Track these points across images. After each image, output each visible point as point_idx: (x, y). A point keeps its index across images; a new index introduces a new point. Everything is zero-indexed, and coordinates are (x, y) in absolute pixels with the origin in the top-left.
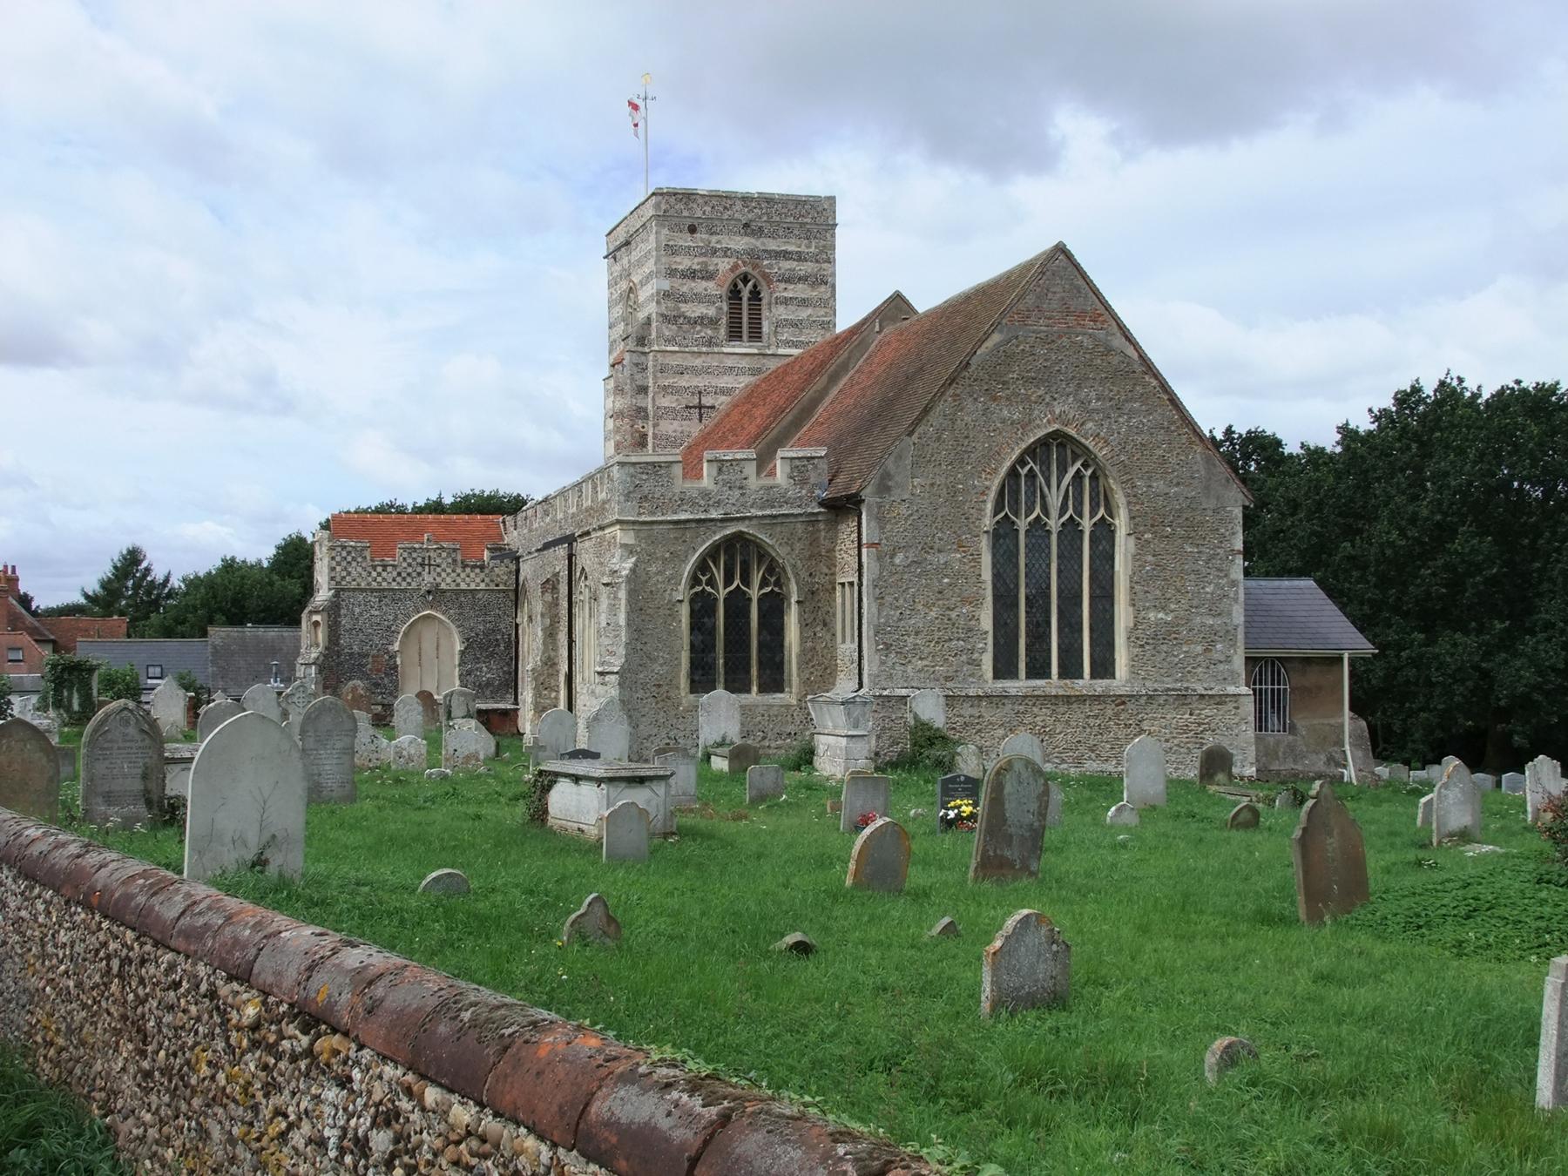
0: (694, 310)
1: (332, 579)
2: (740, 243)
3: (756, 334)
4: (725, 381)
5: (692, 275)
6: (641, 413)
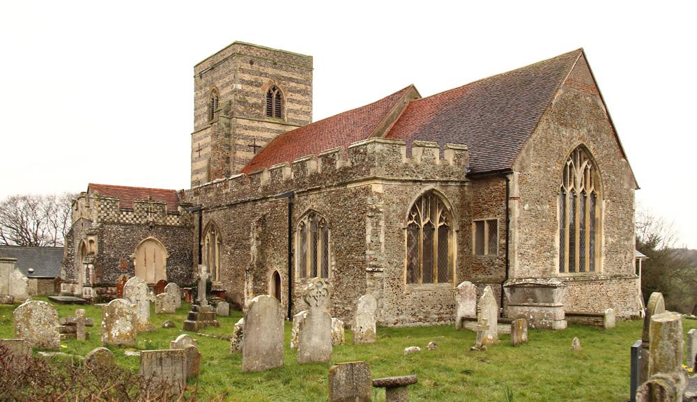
0: (252, 100)
1: (99, 217)
2: (270, 71)
3: (279, 115)
5: (250, 83)
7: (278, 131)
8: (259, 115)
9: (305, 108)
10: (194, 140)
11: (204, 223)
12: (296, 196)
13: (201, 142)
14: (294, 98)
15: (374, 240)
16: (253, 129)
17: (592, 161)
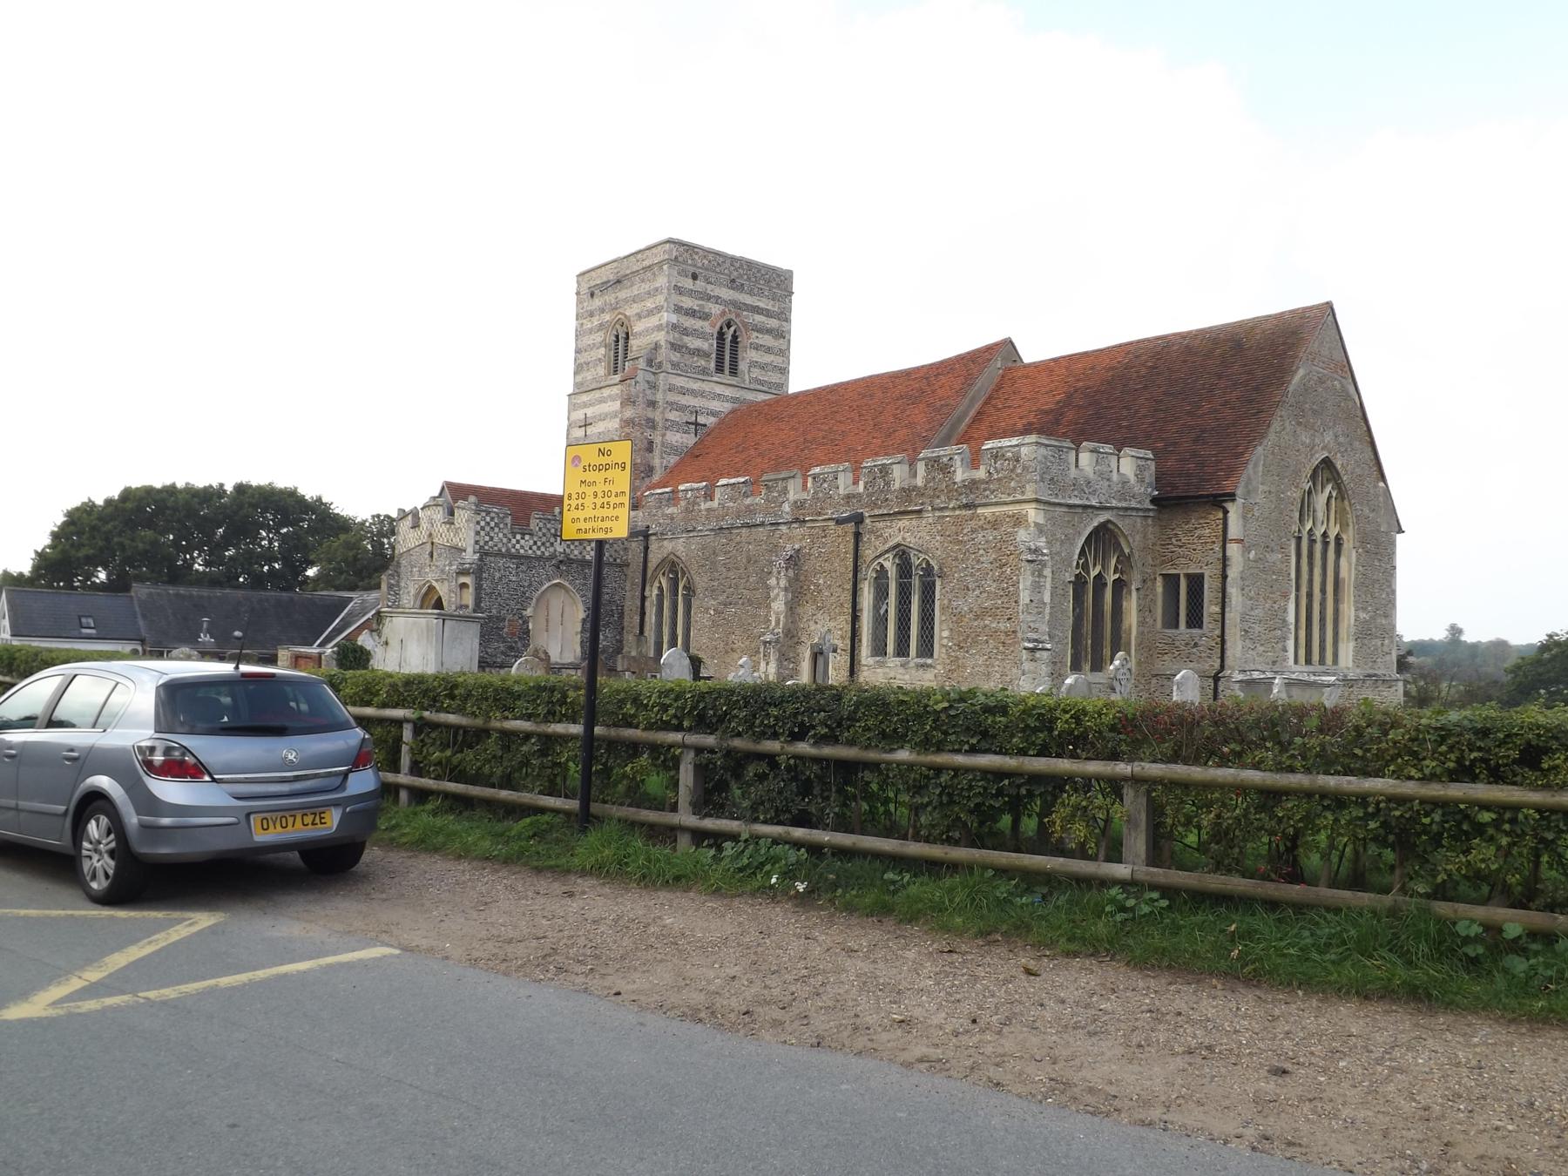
1: (477, 542)
2: (726, 294)
3: (734, 371)
4: (715, 405)
5: (691, 313)
6: (652, 424)
7: (734, 400)
8: (704, 371)
9: (778, 360)
10: (573, 407)
11: (654, 560)
12: (868, 521)
13: (590, 412)
14: (761, 342)
15: (1036, 599)
16: (693, 393)
17: (1339, 486)
